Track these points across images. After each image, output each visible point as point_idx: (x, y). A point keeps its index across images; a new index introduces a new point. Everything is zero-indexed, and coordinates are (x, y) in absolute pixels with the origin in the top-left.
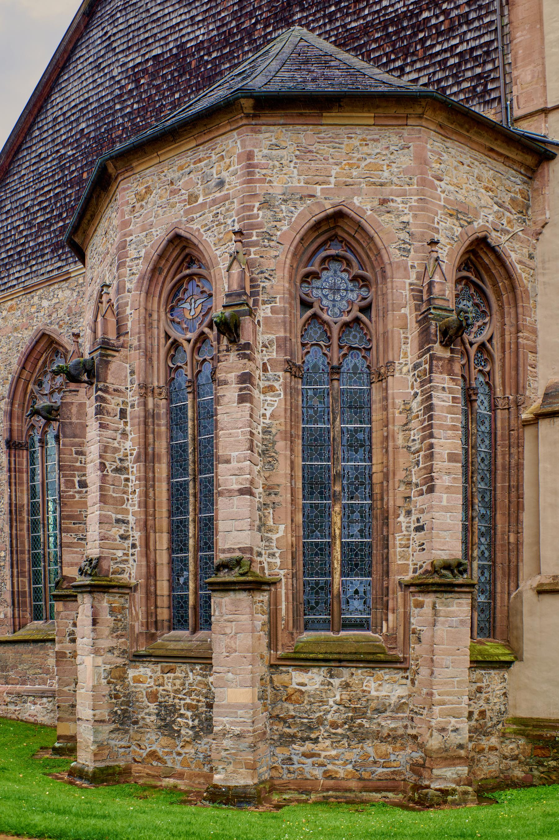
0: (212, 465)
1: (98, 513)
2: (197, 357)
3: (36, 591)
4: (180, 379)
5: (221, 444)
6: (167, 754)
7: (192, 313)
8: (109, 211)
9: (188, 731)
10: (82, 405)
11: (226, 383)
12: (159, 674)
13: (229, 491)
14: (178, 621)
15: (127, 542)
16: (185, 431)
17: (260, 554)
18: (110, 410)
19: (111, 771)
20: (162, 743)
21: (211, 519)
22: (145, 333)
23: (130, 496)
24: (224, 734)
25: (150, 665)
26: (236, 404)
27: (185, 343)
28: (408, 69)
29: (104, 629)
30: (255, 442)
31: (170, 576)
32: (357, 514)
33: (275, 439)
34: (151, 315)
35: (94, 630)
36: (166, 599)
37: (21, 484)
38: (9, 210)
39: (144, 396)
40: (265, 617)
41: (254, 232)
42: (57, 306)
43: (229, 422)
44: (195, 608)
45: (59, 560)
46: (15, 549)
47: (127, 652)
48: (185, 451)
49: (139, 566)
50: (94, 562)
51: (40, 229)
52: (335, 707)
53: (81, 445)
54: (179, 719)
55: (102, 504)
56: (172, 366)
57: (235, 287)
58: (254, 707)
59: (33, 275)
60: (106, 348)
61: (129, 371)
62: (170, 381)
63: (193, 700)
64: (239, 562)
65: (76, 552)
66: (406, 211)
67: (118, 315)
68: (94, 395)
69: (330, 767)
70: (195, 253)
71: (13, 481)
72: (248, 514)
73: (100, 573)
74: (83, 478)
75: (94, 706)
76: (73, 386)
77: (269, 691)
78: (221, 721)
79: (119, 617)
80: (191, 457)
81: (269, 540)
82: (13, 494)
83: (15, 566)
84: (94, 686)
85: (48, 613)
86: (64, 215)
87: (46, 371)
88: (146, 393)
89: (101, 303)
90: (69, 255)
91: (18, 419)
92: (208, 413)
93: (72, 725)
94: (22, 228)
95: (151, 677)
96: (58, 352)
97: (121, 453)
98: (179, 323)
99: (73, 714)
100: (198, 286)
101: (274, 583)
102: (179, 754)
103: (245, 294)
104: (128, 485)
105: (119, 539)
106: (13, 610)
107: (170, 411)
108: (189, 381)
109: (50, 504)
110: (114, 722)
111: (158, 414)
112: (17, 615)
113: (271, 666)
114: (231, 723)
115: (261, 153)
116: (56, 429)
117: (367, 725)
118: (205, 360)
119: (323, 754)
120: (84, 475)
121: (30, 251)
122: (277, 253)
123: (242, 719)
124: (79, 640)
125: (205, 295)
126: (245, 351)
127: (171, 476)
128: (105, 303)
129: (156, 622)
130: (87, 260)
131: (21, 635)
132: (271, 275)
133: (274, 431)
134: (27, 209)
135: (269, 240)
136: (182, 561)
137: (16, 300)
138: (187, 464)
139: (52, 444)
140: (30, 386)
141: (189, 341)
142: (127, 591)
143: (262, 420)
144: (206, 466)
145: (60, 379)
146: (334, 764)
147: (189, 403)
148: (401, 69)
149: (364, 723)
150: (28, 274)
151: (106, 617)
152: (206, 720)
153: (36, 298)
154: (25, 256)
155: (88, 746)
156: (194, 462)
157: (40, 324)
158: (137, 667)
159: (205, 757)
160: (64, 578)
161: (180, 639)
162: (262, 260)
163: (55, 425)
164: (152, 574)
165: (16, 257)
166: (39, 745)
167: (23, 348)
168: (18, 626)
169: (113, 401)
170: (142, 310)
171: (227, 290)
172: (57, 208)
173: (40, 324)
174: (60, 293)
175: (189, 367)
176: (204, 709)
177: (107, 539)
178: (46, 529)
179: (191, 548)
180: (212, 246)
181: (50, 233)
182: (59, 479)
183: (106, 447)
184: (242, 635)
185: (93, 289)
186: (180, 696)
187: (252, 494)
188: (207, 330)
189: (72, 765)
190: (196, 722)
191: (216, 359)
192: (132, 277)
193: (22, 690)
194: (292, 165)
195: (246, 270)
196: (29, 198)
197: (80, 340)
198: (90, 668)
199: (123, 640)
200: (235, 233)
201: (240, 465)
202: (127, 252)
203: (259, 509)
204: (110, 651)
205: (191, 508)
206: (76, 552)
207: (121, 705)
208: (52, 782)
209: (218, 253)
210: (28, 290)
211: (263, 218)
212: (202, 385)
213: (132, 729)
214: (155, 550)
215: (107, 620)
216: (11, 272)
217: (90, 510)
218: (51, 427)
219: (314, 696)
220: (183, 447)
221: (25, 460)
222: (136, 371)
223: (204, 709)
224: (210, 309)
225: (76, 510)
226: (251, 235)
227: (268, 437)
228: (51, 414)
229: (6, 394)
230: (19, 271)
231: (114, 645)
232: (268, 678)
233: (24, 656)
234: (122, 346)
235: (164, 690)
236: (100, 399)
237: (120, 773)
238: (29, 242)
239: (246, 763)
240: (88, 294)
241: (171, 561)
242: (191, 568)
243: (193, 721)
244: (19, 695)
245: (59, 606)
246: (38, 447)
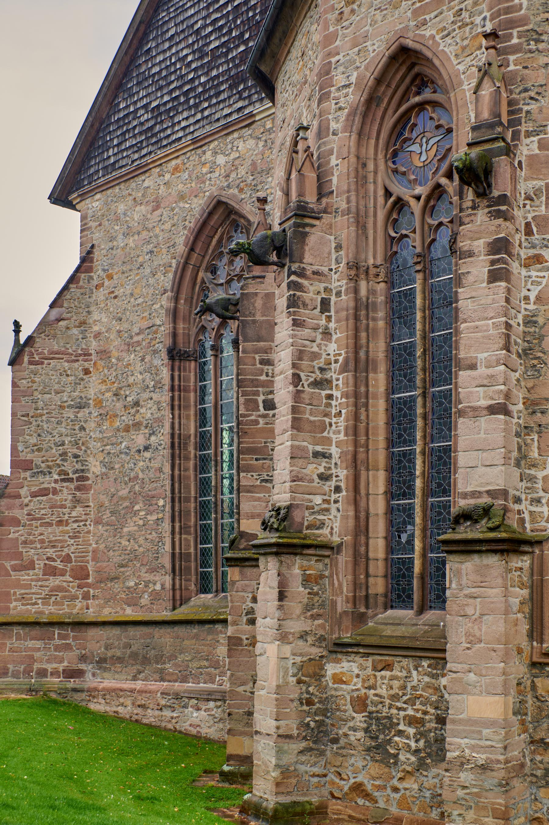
0: (450, 373)
1: (289, 443)
2: (430, 221)
3: (204, 553)
4: (405, 253)
5: (463, 343)
6: (379, 788)
7: (423, 158)
8: (307, 23)
9: (409, 756)
10: (269, 297)
11: (470, 254)
12: (369, 671)
13: (474, 409)
14: (399, 596)
15: (328, 483)
16: (411, 325)
17: (518, 500)
18: (307, 301)
19: (298, 809)
20: (372, 772)
21: (447, 450)
22: (357, 191)
23: (334, 420)
24: (462, 764)
25: (357, 658)
26: (485, 284)
27: (412, 202)
29: (295, 607)
30: (513, 337)
31: (388, 531)
33: (543, 332)
34: (364, 165)
35: (280, 608)
36: (381, 564)
37: (187, 407)
38: (173, 36)
39: (354, 280)
40: (525, 592)
41: (515, 32)
42: (236, 162)
43: (475, 311)
44: (422, 577)
45: (235, 511)
46: (177, 495)
47: (325, 640)
48: (412, 354)
49: (345, 518)
50: (282, 512)
51: (215, 58)
53: (268, 350)
54: (396, 739)
55: (295, 432)
56: (393, 234)
57: (486, 115)
58: (506, 725)
59: (205, 122)
60: (302, 215)
61: (333, 245)
62: (391, 257)
63: (417, 711)
64: (487, 511)
65: (259, 499)
67: (319, 168)
68: (286, 281)
70: (428, 71)
71: (176, 403)
72: (501, 441)
73: (291, 526)
74: (270, 397)
75: (278, 714)
76: (257, 270)
77: (530, 702)
78: (457, 744)
79: (316, 589)
80: (419, 363)
81: (532, 479)
82: (177, 421)
83: (177, 519)
84: (278, 687)
85: (220, 583)
86: (247, 36)
87: (222, 252)
88: (357, 275)
89: (296, 152)
90: (253, 91)
91: (184, 319)
92: (445, 298)
93: (246, 740)
94: (190, 58)
95: (358, 676)
96: (238, 225)
97: (322, 360)
98: (404, 174)
99: (250, 724)
100: (431, 118)
101: (539, 543)
102: (396, 790)
103: (501, 124)
104: (330, 405)
105: (317, 480)
106: (174, 580)
107: (391, 299)
108: (419, 256)
109: (225, 434)
110: (305, 738)
111: (374, 304)
112: (177, 586)
113: (534, 664)
114: (473, 748)
116: (235, 331)
118: (441, 224)
120: (272, 392)
121: (200, 89)
123: (489, 743)
124: (260, 621)
125: (442, 131)
126: (500, 207)
127: (391, 390)
128: (304, 158)
129: (367, 597)
130: (280, 97)
131: (182, 613)
132: (538, 93)
133: (541, 320)
134: (198, 32)
135: (537, 41)
136: (404, 510)
137: (183, 157)
138: (415, 373)
139: (228, 351)
140: (201, 274)
141: (418, 198)
142: (327, 553)
143: (523, 306)
144: (441, 374)
145: (240, 262)
147: (418, 286)
150: (198, 121)
151: (297, 588)
152: (436, 741)
153: (209, 153)
154: (195, 97)
155: (268, 772)
156: (424, 370)
157: (214, 188)
158: (338, 661)
159: (433, 796)
160: (242, 535)
161: (399, 622)
162: (526, 71)
163: (233, 325)
164: (363, 528)
165: (182, 99)
166: (202, 768)
167: (192, 223)
168: (179, 600)
169: (312, 288)
170: (353, 159)
171: (473, 120)
172: (237, 27)
173: (214, 188)
174: (241, 145)
175: (418, 236)
176: (433, 725)
177: (301, 480)
178: (219, 468)
179: (418, 492)
180: (453, 58)
181: (227, 62)
182: (238, 398)
183: (301, 352)
184: (490, 618)
185: (284, 136)
186: (399, 704)
187: (507, 413)
188: (444, 181)
189: (246, 797)
190: (421, 744)
191: (457, 221)
192: (339, 113)
193: (182, 689)
195: (503, 90)
196: (200, 16)
197: (267, 208)
198: (273, 660)
199: (320, 621)
200: (486, 36)
201: (490, 371)
202: (332, 78)
203: (518, 435)
204: (301, 637)
205: (419, 435)
206: (259, 499)
207: (316, 714)
208: (218, 821)
209: (461, 68)
210: (199, 143)
211: (528, 9)
212: (437, 261)
213: (330, 750)
214: (368, 494)
215: (299, 593)
216: (176, 120)
217: (278, 441)
218: (228, 329)
220: (409, 349)
221: (192, 374)
222: (344, 245)
223: (433, 725)
224: (449, 150)
225: (260, 441)
226: (510, 37)
227: (532, 330)
228: (227, 310)
229: (168, 286)
230: (187, 118)
231: (308, 629)
232: (529, 682)
233: (186, 642)
234: (325, 211)
235: (376, 695)
236: (293, 285)
237: (311, 813)
238: (199, 77)
239: (493, 810)
240: (278, 142)
241: (390, 510)
242: (418, 520)
243: (417, 741)
244: (177, 696)
245: (233, 573)
246: (209, 357)
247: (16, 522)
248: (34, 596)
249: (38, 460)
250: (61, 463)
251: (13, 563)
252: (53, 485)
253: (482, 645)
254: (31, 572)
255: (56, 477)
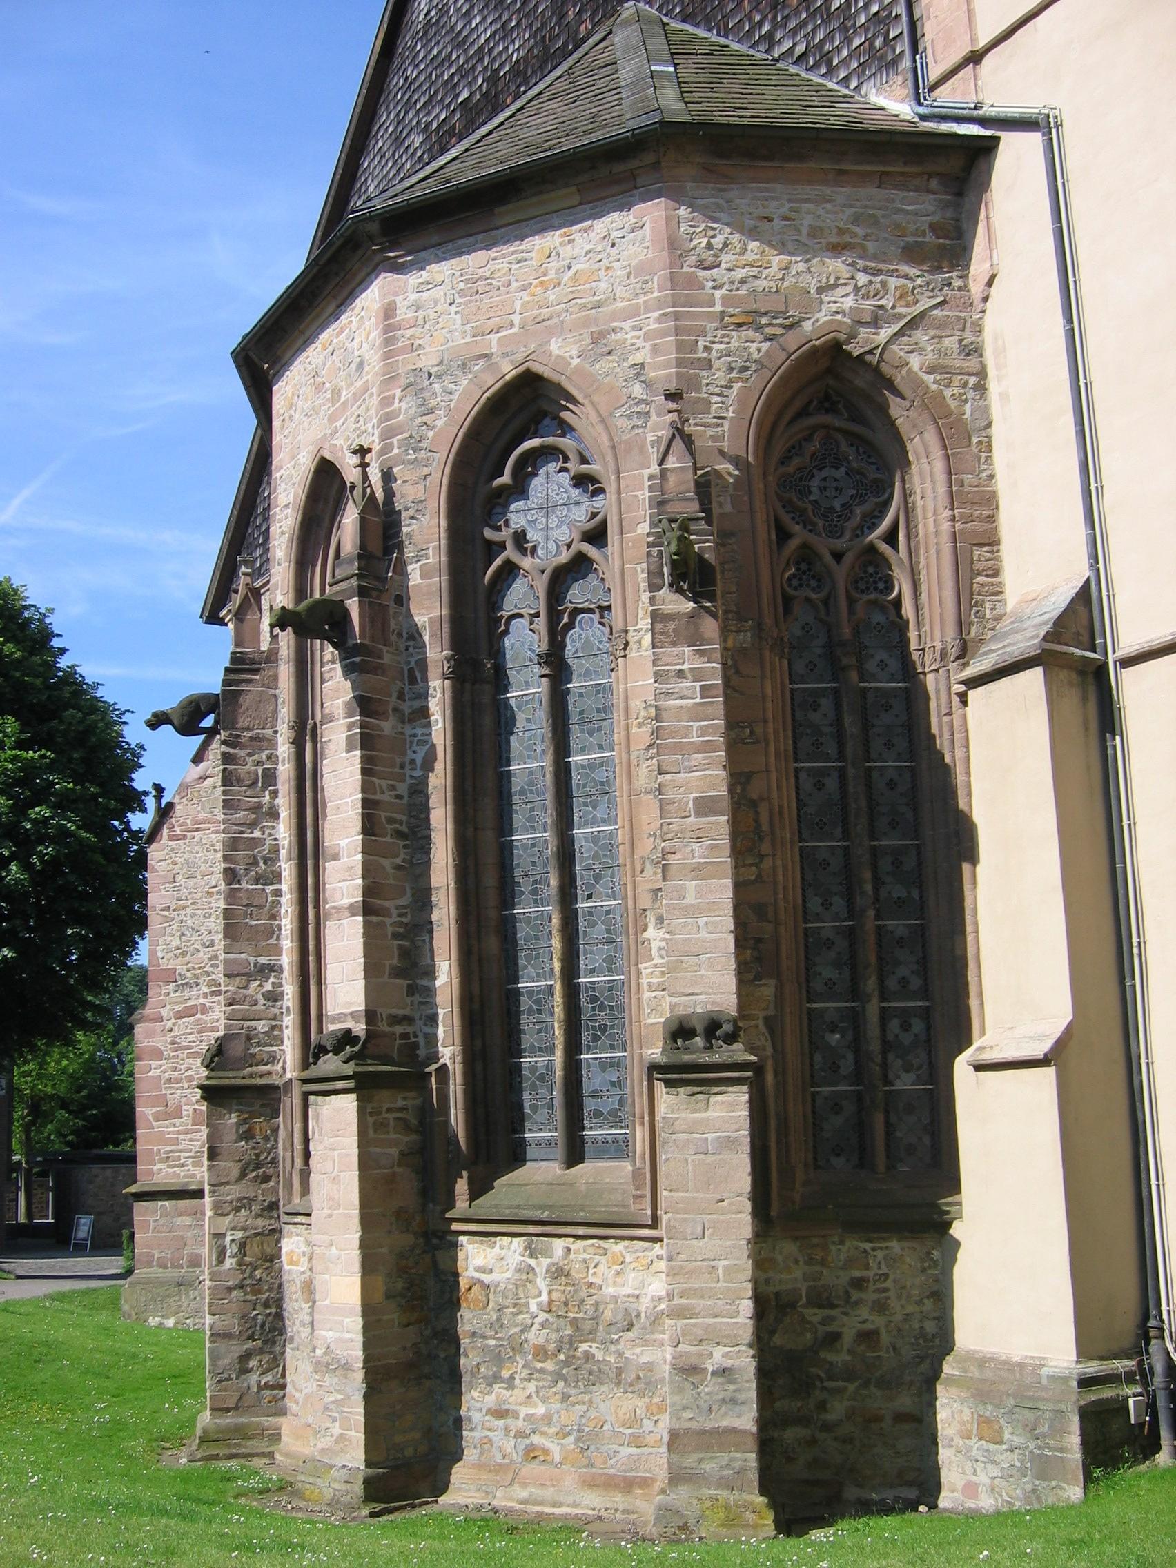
28: (778, 36)
32: (601, 927)
41: (395, 440)
52: (543, 1316)
66: (640, 343)
69: (536, 1439)
97: (266, 847)
115: (405, 303)
117: (599, 1356)
119: (523, 1411)
122: (426, 471)
146: (542, 1433)
148: (770, 36)
149: (593, 1351)
194: (454, 308)
219: (504, 1293)
247: (158, 1054)
248: (183, 1154)
249: (182, 969)
250: (211, 969)
251: (155, 1110)
252: (202, 1001)
253: (341, 1211)
254: (178, 1121)
255: (205, 990)
